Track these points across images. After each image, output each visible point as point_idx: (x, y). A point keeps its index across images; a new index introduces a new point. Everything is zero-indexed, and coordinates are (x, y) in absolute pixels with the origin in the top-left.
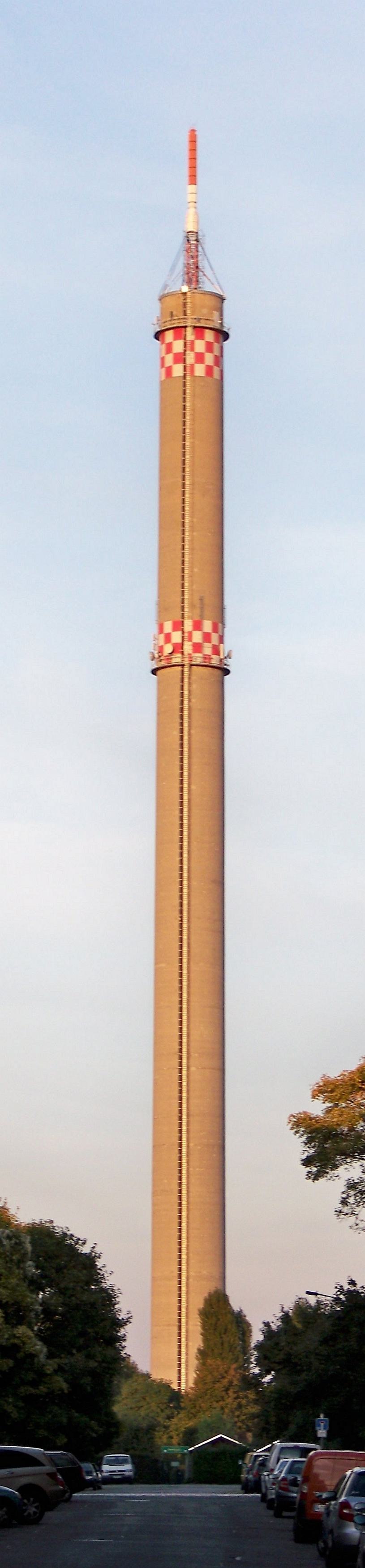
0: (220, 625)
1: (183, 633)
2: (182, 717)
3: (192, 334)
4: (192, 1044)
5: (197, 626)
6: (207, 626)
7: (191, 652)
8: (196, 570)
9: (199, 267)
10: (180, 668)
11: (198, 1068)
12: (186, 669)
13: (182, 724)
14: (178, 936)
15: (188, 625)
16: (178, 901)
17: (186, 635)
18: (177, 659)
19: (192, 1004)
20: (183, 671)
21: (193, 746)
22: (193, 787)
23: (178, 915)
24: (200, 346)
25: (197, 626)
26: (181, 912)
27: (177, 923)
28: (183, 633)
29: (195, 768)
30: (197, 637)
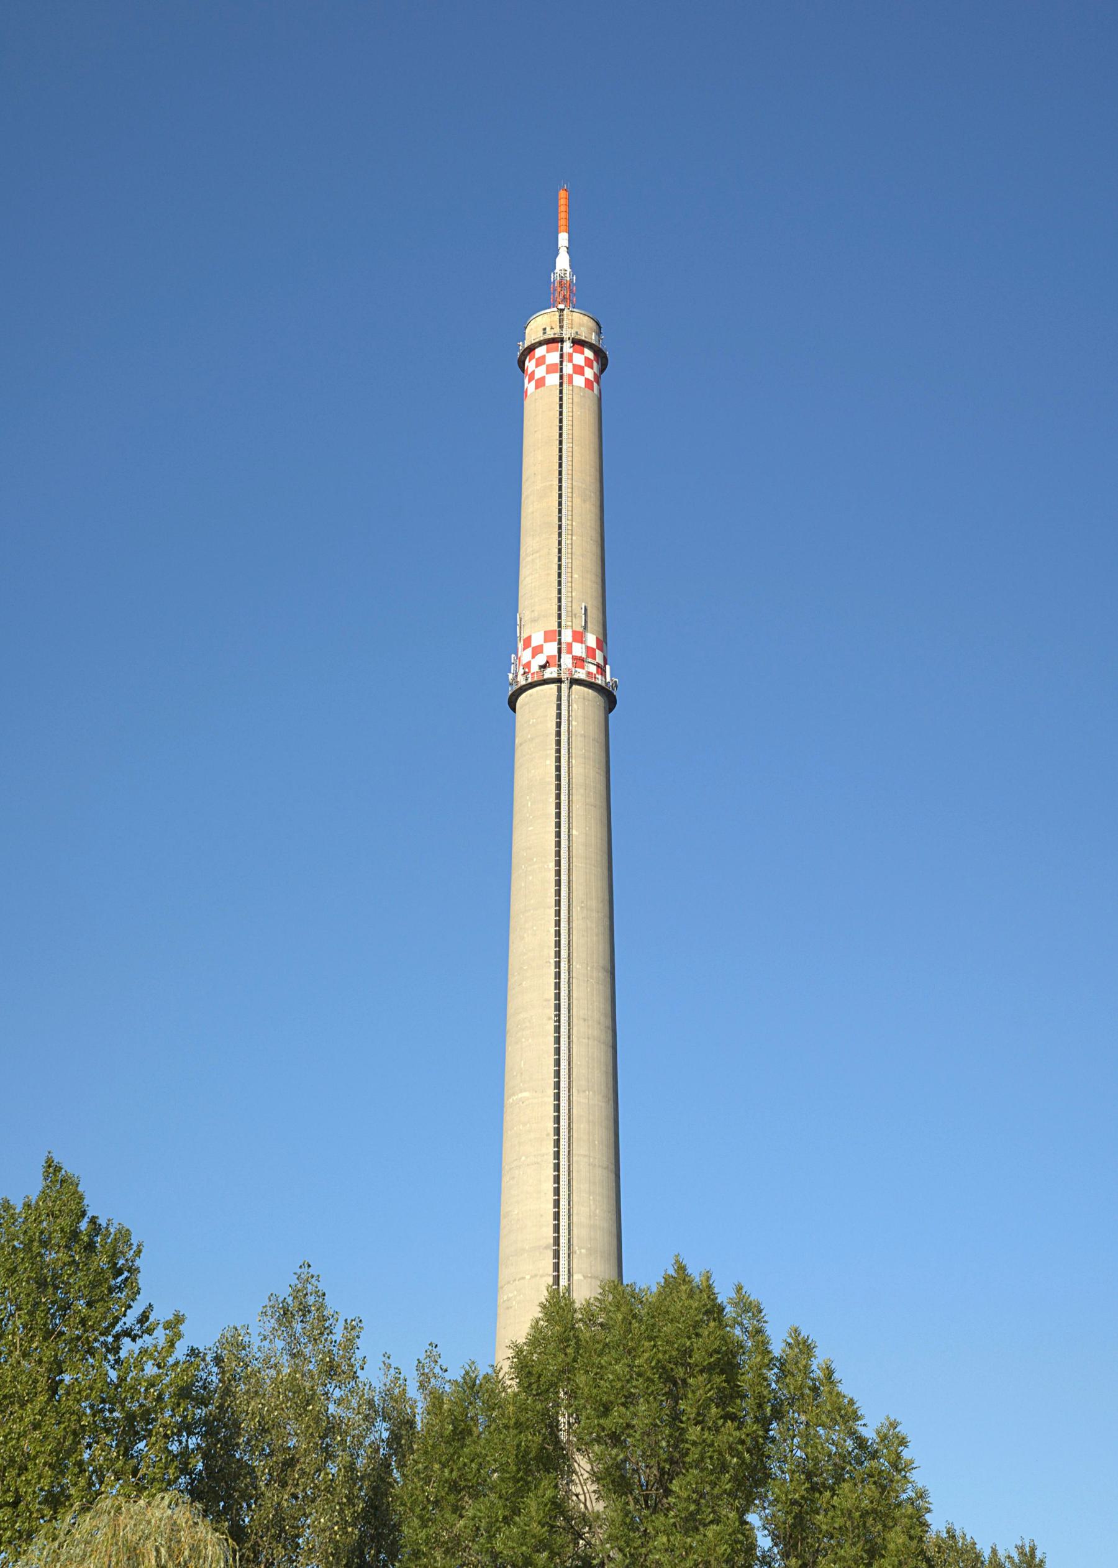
0: (604, 645)
1: (560, 643)
2: (558, 743)
3: (607, 1168)
4: (575, 1231)
5: (579, 637)
6: (591, 640)
7: (570, 666)
8: (575, 576)
9: (284, 1292)
10: (554, 686)
11: (585, 1277)
12: (565, 686)
13: (558, 751)
14: (552, 1046)
15: (567, 636)
16: (552, 992)
17: (564, 646)
18: (551, 673)
19: (575, 1159)
20: (559, 690)
21: (574, 852)
22: (574, 832)
23: (552, 1012)
24: (579, 359)
25: (579, 637)
26: (558, 1007)
27: (551, 1025)
28: (560, 643)
29: (575, 807)
30: (579, 650)
